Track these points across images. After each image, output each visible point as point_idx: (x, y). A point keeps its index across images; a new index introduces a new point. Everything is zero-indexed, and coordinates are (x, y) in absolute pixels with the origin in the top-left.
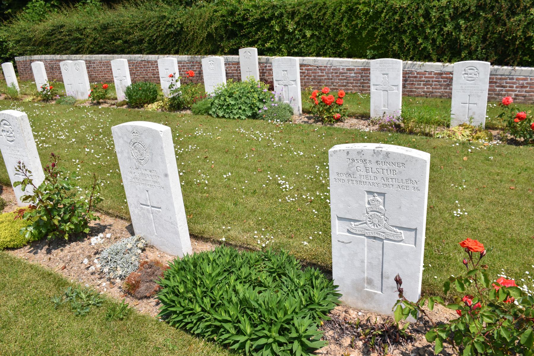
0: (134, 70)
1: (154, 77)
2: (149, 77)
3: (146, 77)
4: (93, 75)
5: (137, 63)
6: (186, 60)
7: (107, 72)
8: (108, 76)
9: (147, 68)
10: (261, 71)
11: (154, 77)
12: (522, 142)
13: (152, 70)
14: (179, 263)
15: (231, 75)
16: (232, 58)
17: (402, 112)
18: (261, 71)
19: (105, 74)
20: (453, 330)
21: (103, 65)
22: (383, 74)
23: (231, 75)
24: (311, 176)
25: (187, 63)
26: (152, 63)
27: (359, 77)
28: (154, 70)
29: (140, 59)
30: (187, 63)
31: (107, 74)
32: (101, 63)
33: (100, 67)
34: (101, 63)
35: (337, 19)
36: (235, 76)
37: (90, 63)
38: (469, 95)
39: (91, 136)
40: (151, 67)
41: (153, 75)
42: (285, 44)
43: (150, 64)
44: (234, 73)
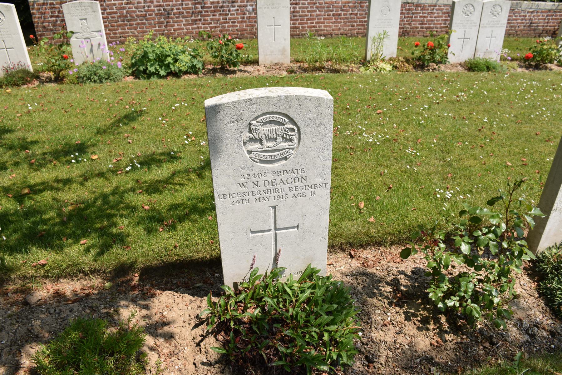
1: (422, 28)
2: (413, 28)
3: (408, 28)
8: (325, 26)
9: (413, 14)
10: (292, 10)
11: (422, 28)
12: (84, 208)
13: (421, 17)
14: (471, 64)
15: (535, 25)
18: (292, 10)
21: (317, 7)
22: (81, 19)
23: (535, 25)
26: (424, 6)
28: (424, 17)
31: (323, 23)
35: (131, 183)
36: (541, 26)
38: (274, 208)
40: (420, 13)
41: (420, 24)
42: (512, 262)
43: (419, 8)
44: (540, 23)
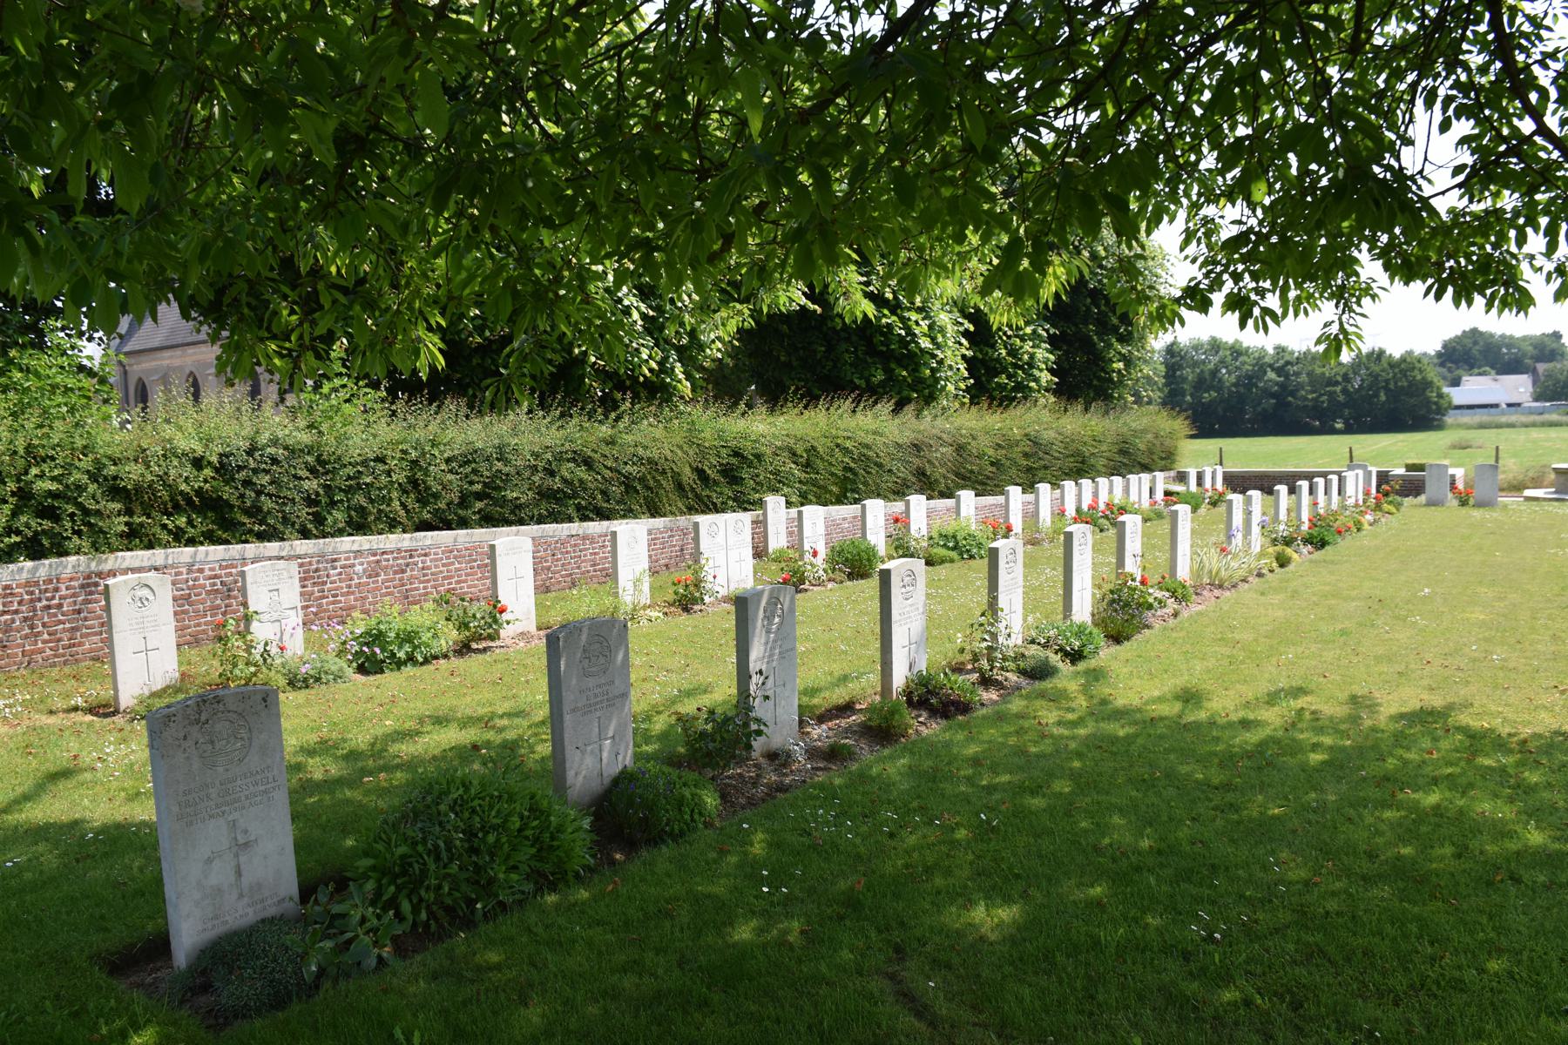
0: (546, 561)
4: (417, 589)
5: (557, 542)
6: (661, 526)
7: (467, 575)
8: (469, 587)
16: (898, 507)
17: (1518, 853)
19: (458, 582)
20: (629, 395)
21: (455, 557)
24: (1556, 554)
25: (661, 533)
27: (17, 654)
29: (566, 533)
30: (661, 533)
32: (451, 551)
33: (444, 565)
34: (451, 551)
37: (411, 556)
39: (1151, 75)
